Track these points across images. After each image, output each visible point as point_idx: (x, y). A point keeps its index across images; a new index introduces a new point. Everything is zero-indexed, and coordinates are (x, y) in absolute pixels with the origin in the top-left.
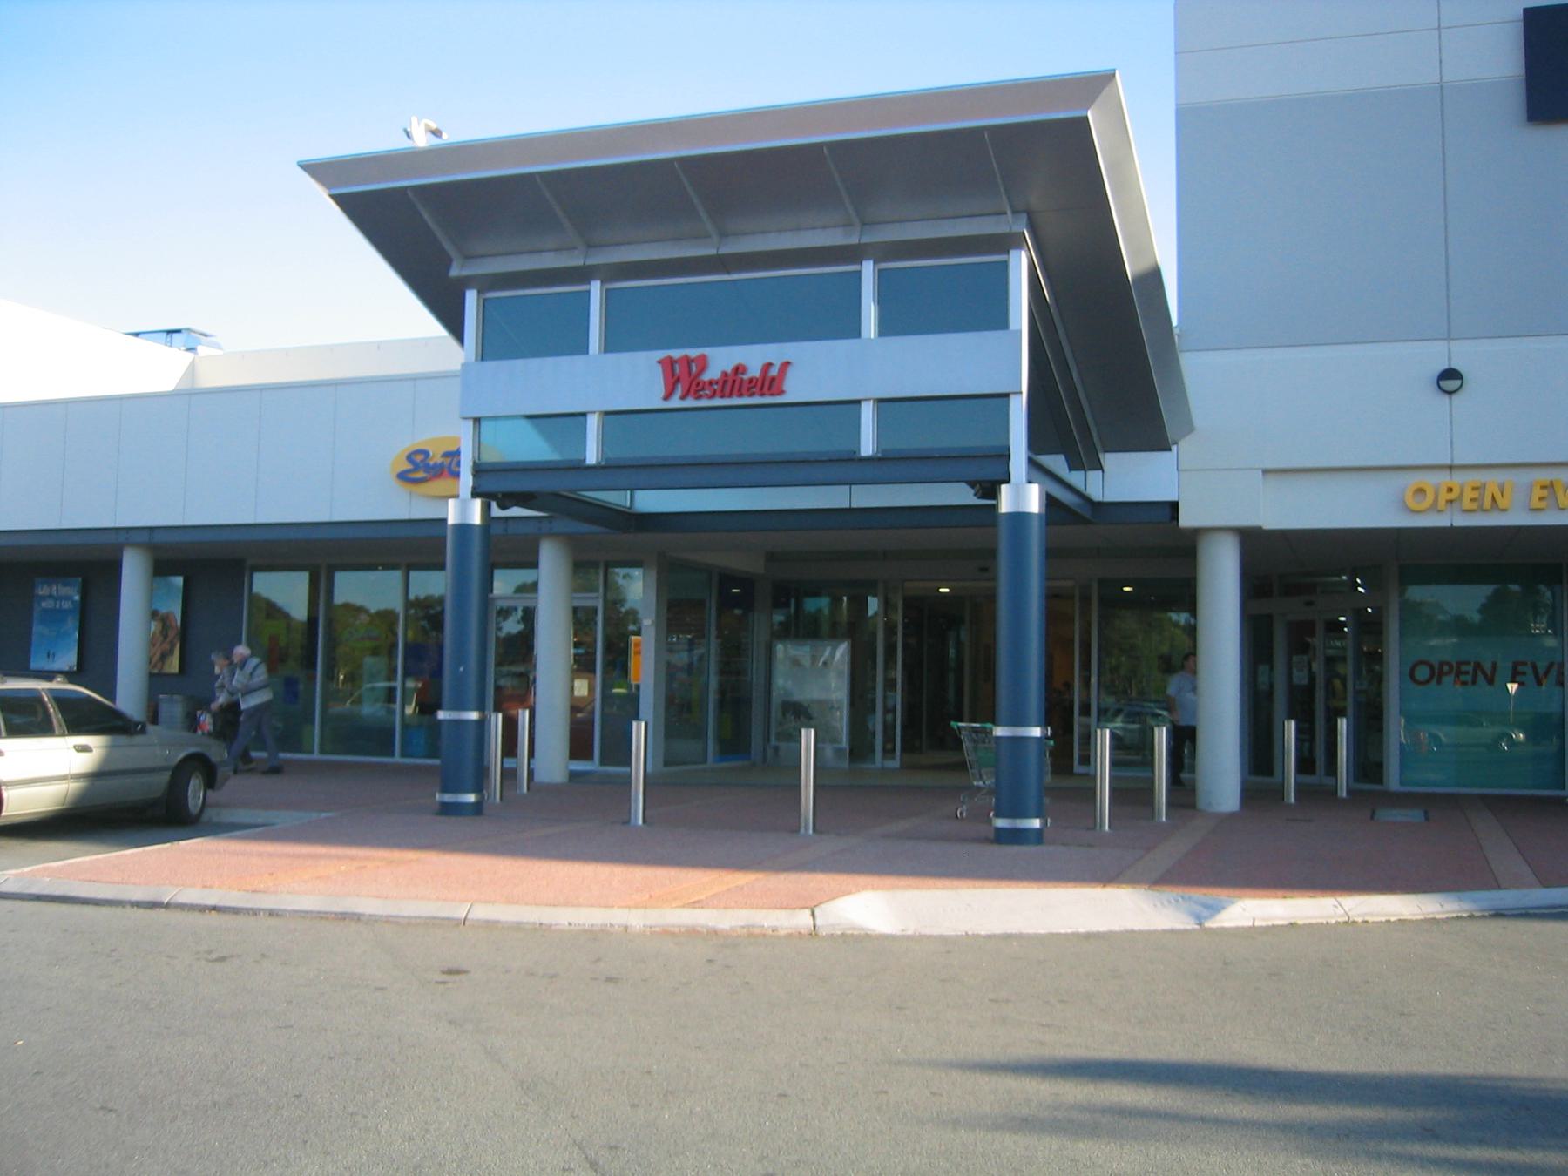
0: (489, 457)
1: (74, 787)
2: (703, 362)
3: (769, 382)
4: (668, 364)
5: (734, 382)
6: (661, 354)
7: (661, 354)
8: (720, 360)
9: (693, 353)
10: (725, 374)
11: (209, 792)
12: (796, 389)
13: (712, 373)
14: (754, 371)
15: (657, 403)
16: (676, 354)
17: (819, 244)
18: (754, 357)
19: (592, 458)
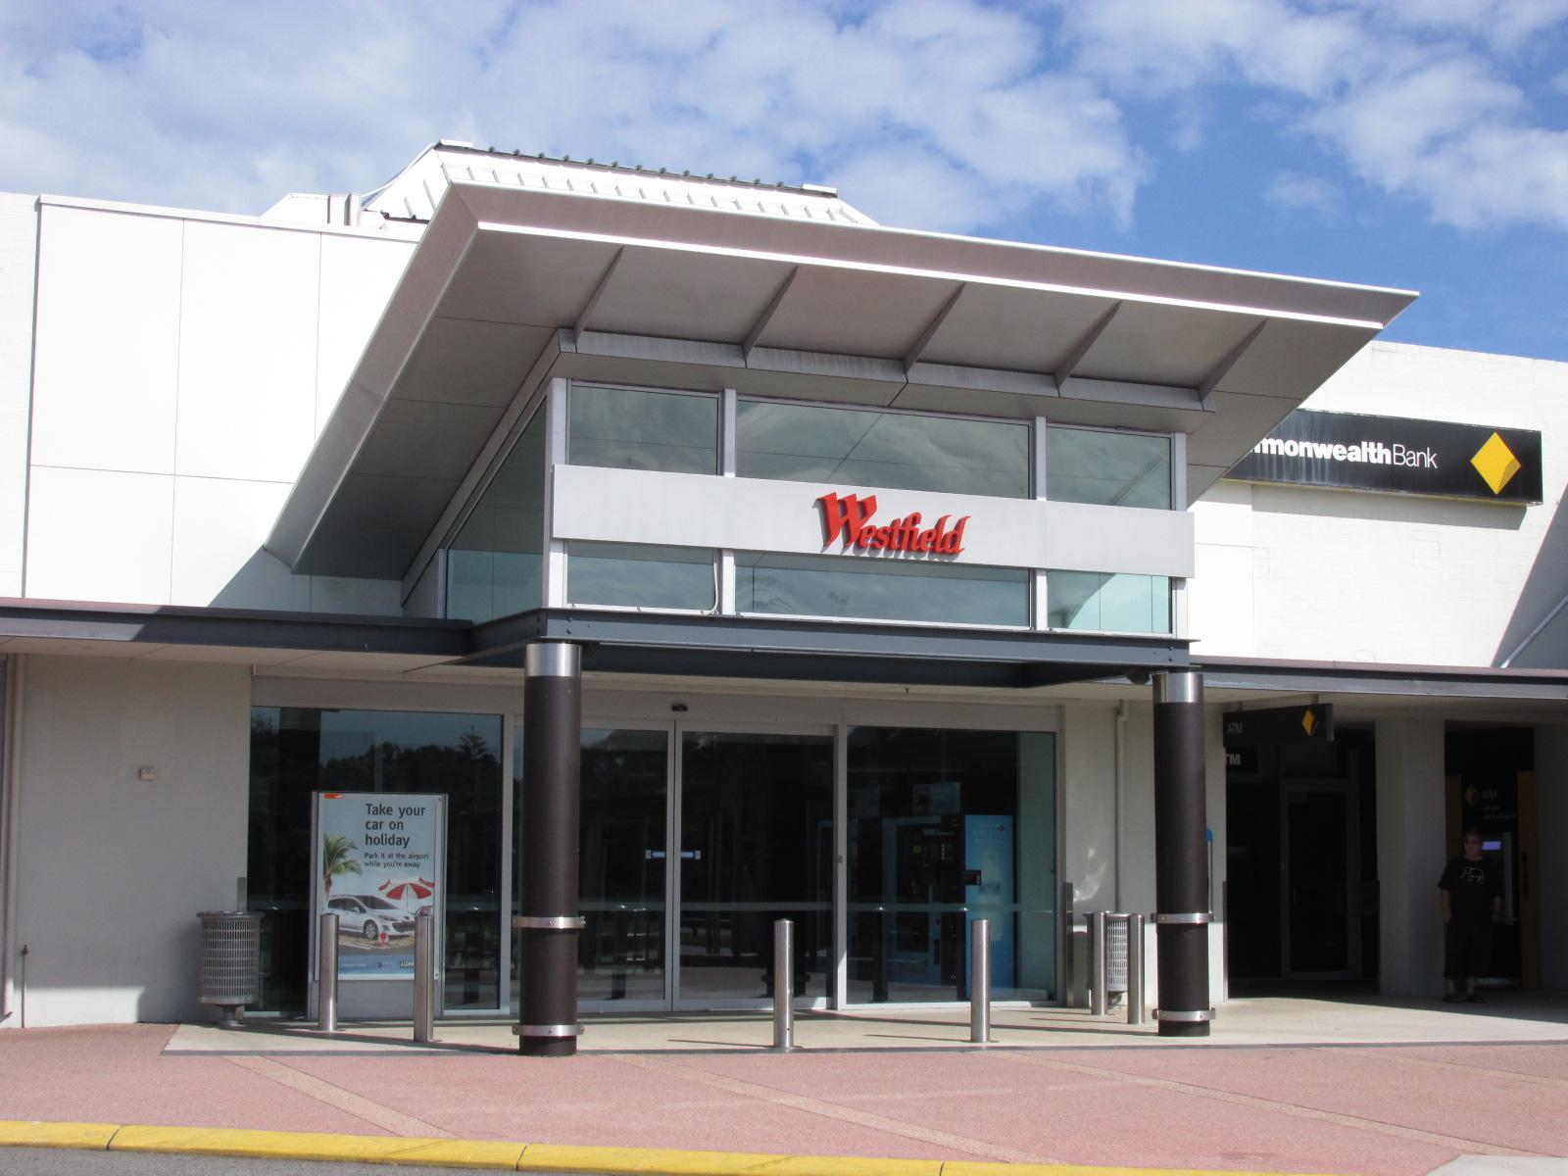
0: (1126, 1021)
1: (612, 732)
2: (867, 508)
3: (946, 541)
4: (823, 504)
5: (903, 534)
6: (824, 490)
7: (824, 490)
8: (891, 506)
9: (862, 493)
10: (895, 523)
11: (243, 1008)
12: (971, 552)
13: (879, 520)
14: (925, 526)
15: (818, 551)
16: (843, 492)
17: (504, 824)
18: (931, 508)
19: (411, 976)
